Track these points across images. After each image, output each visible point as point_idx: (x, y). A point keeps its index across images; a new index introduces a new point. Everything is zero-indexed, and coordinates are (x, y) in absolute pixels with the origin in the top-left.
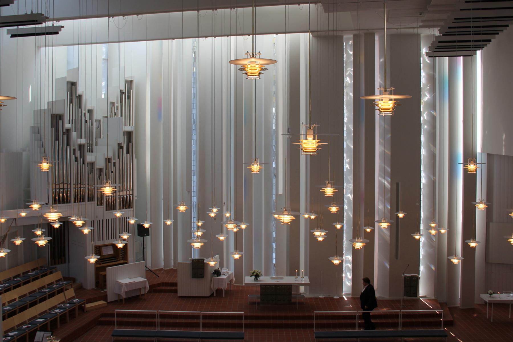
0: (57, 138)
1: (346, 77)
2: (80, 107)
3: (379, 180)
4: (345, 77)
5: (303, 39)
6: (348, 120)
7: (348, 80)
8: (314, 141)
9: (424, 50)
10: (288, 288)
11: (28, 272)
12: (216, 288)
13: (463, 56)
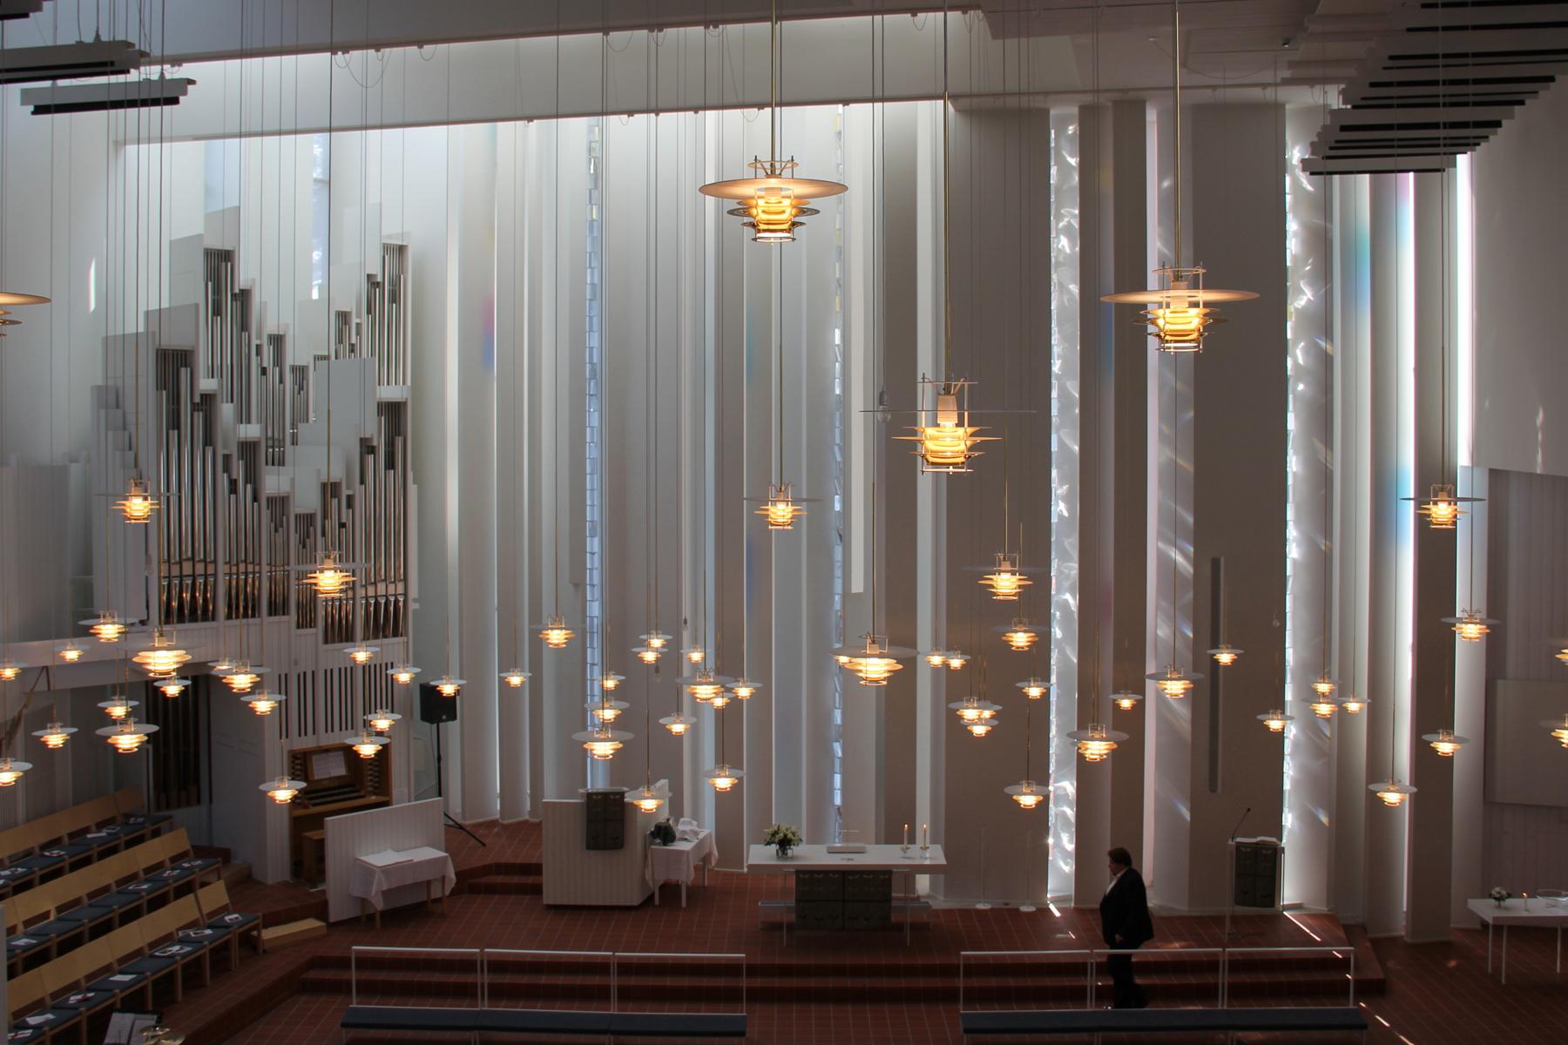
0: (175, 423)
1: (1057, 236)
2: (244, 326)
3: (1158, 549)
4: (1053, 235)
5: (927, 120)
6: (1062, 367)
7: (1064, 245)
8: (961, 431)
9: (1296, 154)
10: (881, 879)
11: (87, 830)
12: (661, 879)
13: (1415, 171)
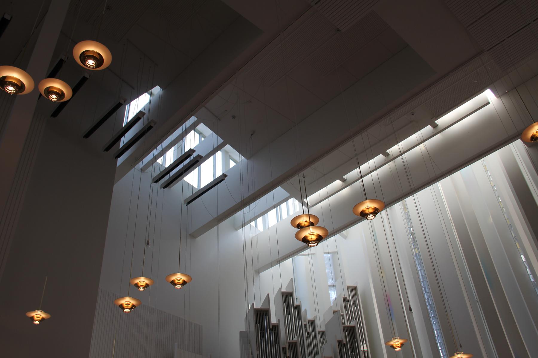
2: (299, 318)
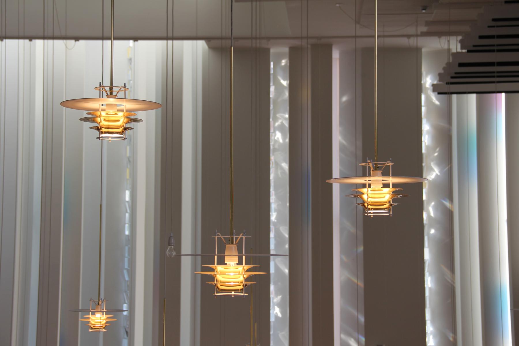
1: (274, 132)
3: (341, 339)
4: (272, 130)
5: (192, 53)
6: (277, 218)
7: (279, 138)
8: (240, 268)
9: (428, 81)
13: (506, 92)
